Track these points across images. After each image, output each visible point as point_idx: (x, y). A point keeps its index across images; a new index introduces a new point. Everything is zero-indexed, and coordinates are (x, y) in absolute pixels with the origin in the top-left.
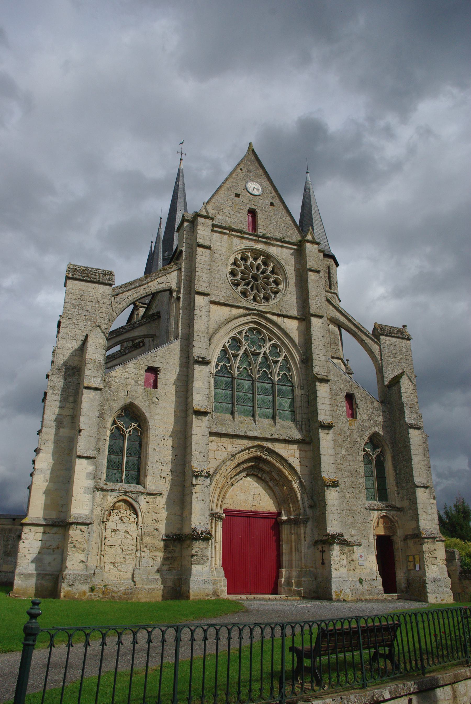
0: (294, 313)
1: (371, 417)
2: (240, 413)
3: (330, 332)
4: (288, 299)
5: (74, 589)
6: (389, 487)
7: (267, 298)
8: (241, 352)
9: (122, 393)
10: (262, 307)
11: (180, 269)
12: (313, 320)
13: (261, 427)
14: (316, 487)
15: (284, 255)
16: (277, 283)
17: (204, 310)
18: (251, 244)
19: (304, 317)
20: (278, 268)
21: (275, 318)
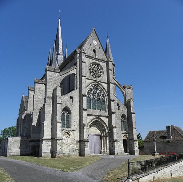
2: (93, 109)
3: (114, 87)
4: (104, 77)
5: (59, 155)
7: (98, 77)
8: (92, 92)
9: (64, 104)
10: (98, 79)
11: (77, 68)
13: (97, 112)
14: (111, 128)
15: (103, 65)
16: (101, 73)
17: (84, 81)
18: (95, 61)
20: (101, 68)
21: (101, 83)
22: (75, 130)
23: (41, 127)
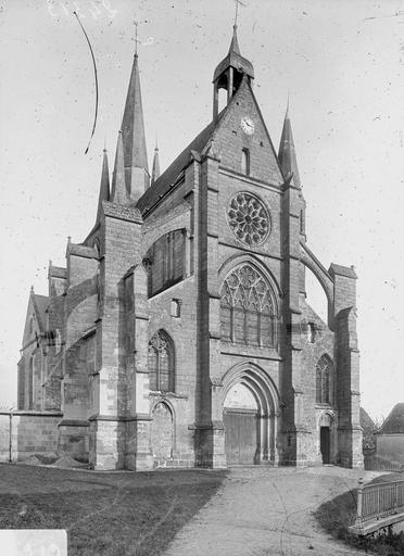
0: (279, 255)
6: (304, 451)
12: (292, 261)
19: (285, 259)
20: (265, 213)
21: (261, 258)
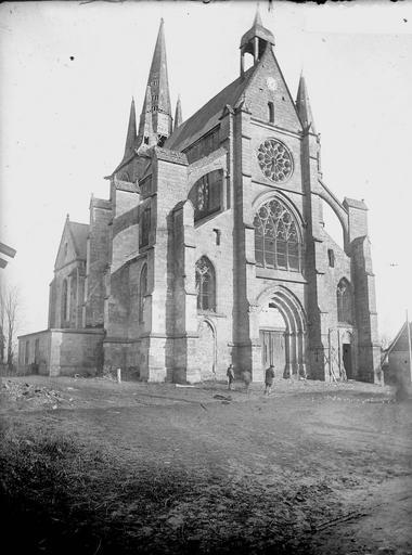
1: (343, 265)
10: (280, 184)
20: (288, 155)
22: (218, 243)
23: (161, 491)
